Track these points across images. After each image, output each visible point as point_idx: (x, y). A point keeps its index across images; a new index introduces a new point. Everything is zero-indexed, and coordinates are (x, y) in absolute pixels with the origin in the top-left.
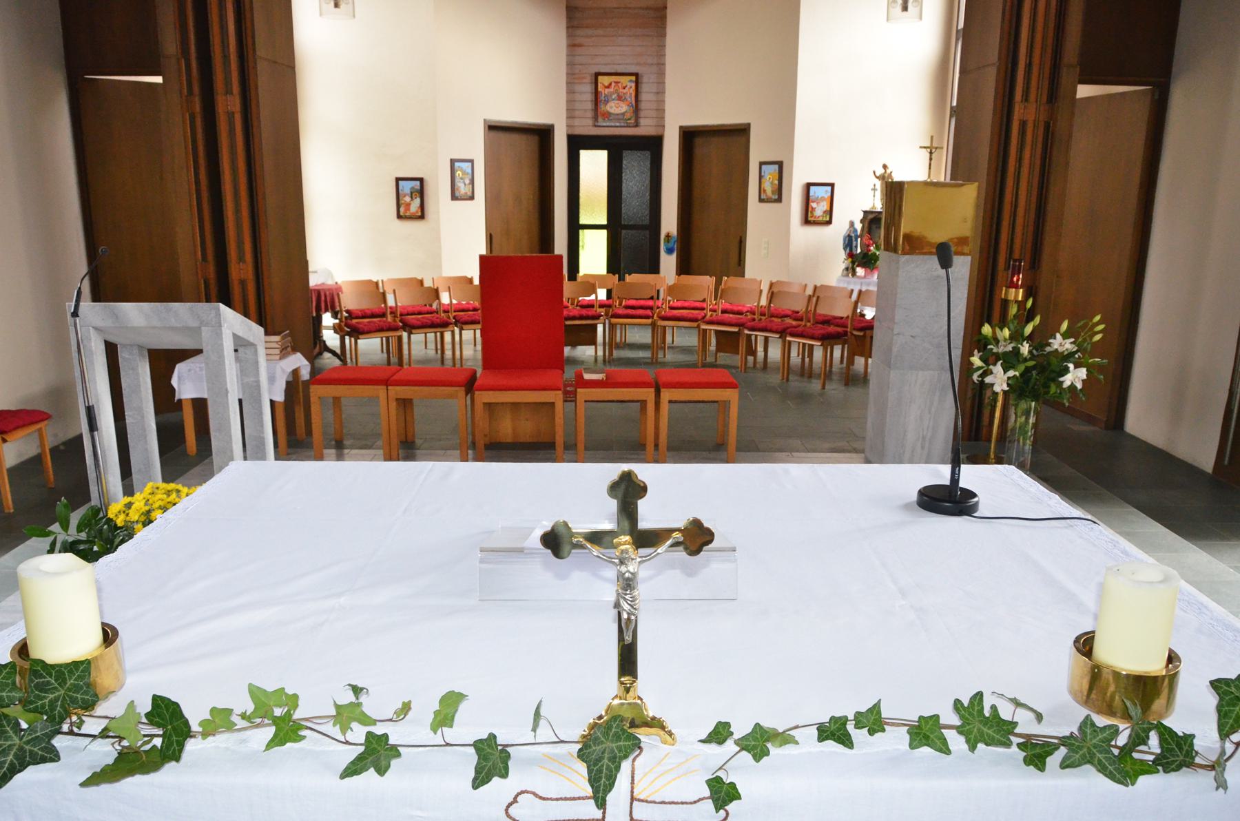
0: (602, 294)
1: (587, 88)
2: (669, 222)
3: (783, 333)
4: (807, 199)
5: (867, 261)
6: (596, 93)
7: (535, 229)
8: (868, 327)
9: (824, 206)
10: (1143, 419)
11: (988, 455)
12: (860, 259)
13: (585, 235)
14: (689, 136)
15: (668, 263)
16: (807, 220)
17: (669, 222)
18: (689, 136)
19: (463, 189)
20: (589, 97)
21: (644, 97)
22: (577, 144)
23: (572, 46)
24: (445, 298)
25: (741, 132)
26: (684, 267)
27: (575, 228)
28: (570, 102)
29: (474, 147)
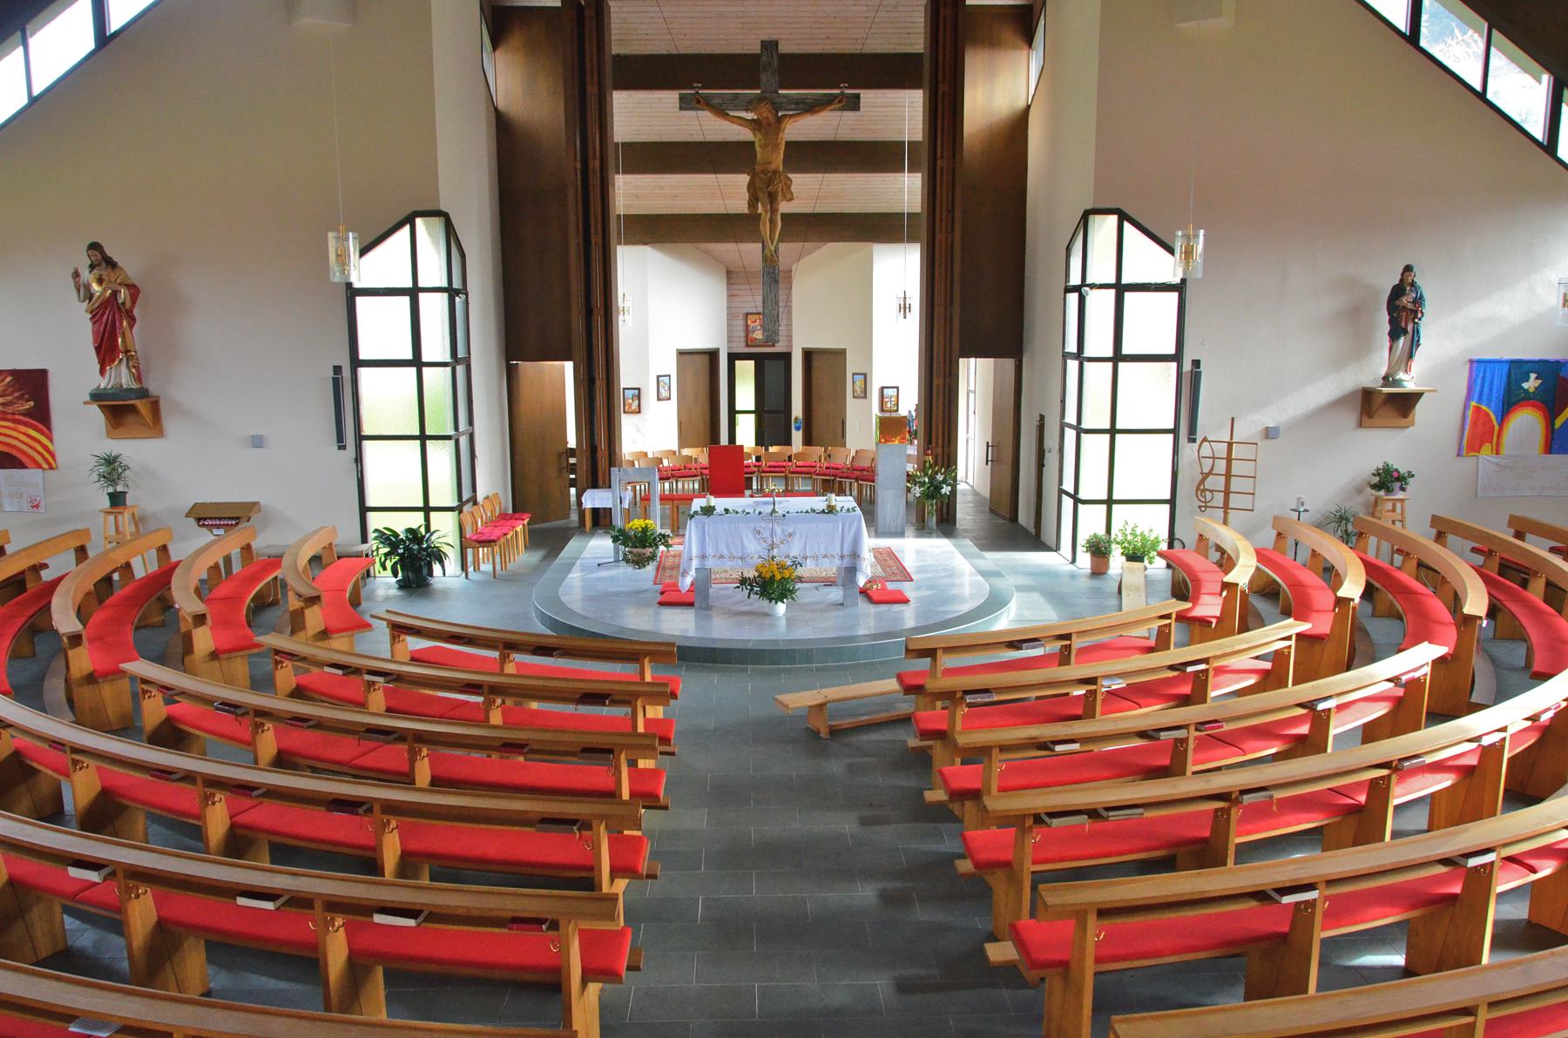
0: (1362, 798)
1: (741, 322)
2: (797, 409)
3: (857, 479)
6: (747, 326)
7: (708, 413)
13: (739, 417)
14: (808, 355)
15: (797, 436)
17: (797, 409)
18: (808, 355)
19: (664, 394)
20: (742, 328)
22: (733, 358)
23: (730, 296)
24: (665, 463)
25: (840, 354)
26: (808, 441)
27: (733, 413)
28: (729, 332)
29: (670, 366)
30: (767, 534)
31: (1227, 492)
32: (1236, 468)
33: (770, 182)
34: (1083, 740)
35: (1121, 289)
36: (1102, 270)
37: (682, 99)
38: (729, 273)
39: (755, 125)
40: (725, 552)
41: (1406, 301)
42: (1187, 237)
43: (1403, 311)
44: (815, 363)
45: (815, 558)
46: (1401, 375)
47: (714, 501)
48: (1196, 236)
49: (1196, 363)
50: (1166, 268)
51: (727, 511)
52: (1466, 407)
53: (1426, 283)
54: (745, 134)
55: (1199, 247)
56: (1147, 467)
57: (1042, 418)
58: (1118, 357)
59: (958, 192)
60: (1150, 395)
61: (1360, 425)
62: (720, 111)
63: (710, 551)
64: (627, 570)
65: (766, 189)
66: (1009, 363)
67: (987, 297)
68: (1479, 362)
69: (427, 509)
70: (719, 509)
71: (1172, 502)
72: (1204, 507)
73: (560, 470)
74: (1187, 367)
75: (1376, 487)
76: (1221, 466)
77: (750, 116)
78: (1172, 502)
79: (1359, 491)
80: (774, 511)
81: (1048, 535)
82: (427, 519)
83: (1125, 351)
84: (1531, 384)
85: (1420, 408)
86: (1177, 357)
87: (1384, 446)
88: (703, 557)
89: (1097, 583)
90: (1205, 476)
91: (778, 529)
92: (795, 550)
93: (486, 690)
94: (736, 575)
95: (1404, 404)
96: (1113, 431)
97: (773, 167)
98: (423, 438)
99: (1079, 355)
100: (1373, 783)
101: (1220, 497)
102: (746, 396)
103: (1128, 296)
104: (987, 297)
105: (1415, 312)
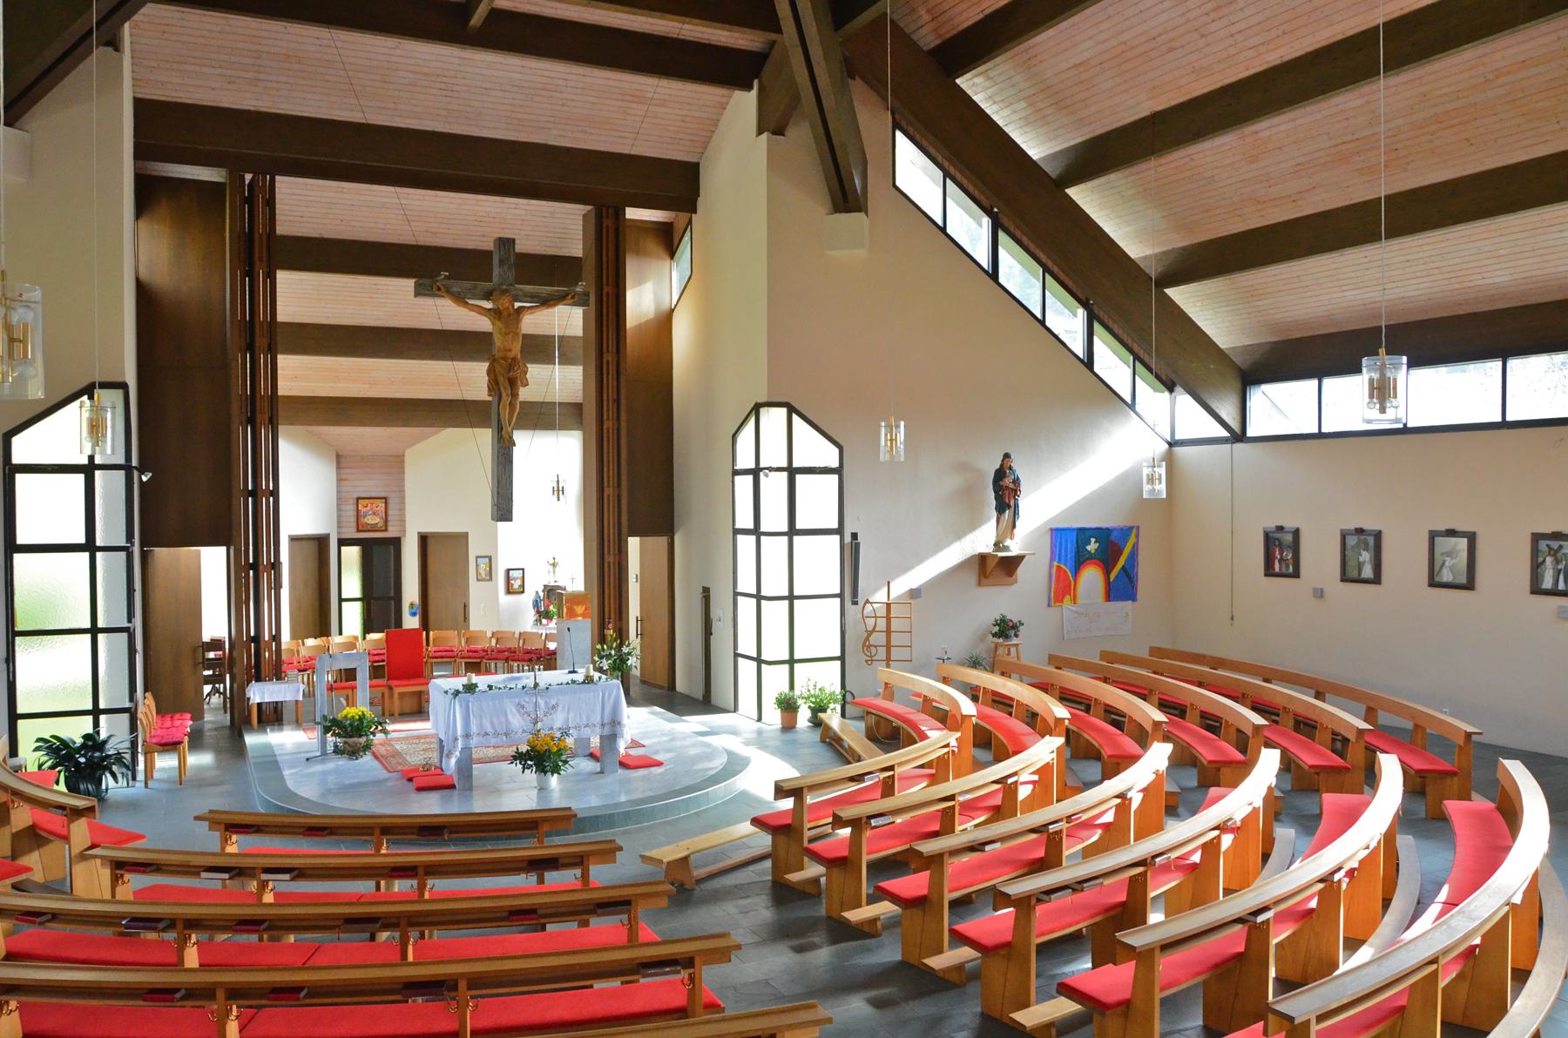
3: (507, 660)
4: (508, 579)
5: (547, 615)
8: (554, 653)
9: (519, 582)
10: (680, 686)
11: (1028, 995)
12: (543, 615)
14: (424, 539)
16: (509, 591)
21: (390, 512)
23: (339, 480)
25: (463, 537)
30: (530, 708)
31: (888, 646)
32: (895, 625)
33: (510, 368)
34: (1002, 839)
35: (792, 472)
36: (774, 455)
37: (417, 286)
38: (338, 457)
39: (495, 314)
40: (489, 729)
41: (1008, 481)
42: (889, 427)
43: (1006, 494)
44: (430, 542)
45: (578, 727)
46: (1008, 542)
47: (475, 679)
48: (898, 426)
49: (855, 536)
50: (830, 457)
51: (490, 687)
52: (1051, 567)
53: (1020, 468)
54: (483, 324)
55: (901, 436)
56: (820, 628)
57: (706, 590)
58: (792, 531)
59: (623, 386)
60: (820, 563)
61: (980, 584)
62: (460, 299)
63: (474, 729)
64: (343, 762)
65: (506, 377)
66: (662, 541)
67: (641, 483)
68: (1057, 530)
69: (96, 712)
70: (482, 686)
71: (842, 658)
72: (870, 661)
73: (195, 665)
74: (848, 539)
75: (995, 635)
76: (882, 624)
77: (488, 305)
78: (842, 658)
79: (982, 639)
80: (536, 685)
81: (722, 692)
82: (96, 724)
83: (751, 526)
84: (1092, 547)
85: (1021, 570)
86: (839, 531)
87: (1000, 601)
88: (467, 736)
89: (789, 736)
90: (870, 633)
91: (541, 702)
92: (558, 720)
93: (421, 871)
94: (511, 751)
95: (1010, 565)
96: (791, 598)
97: (512, 355)
98: (94, 631)
99: (756, 531)
100: (1204, 846)
101: (882, 653)
102: (352, 584)
103: (799, 477)
104: (641, 483)
105: (1015, 491)
